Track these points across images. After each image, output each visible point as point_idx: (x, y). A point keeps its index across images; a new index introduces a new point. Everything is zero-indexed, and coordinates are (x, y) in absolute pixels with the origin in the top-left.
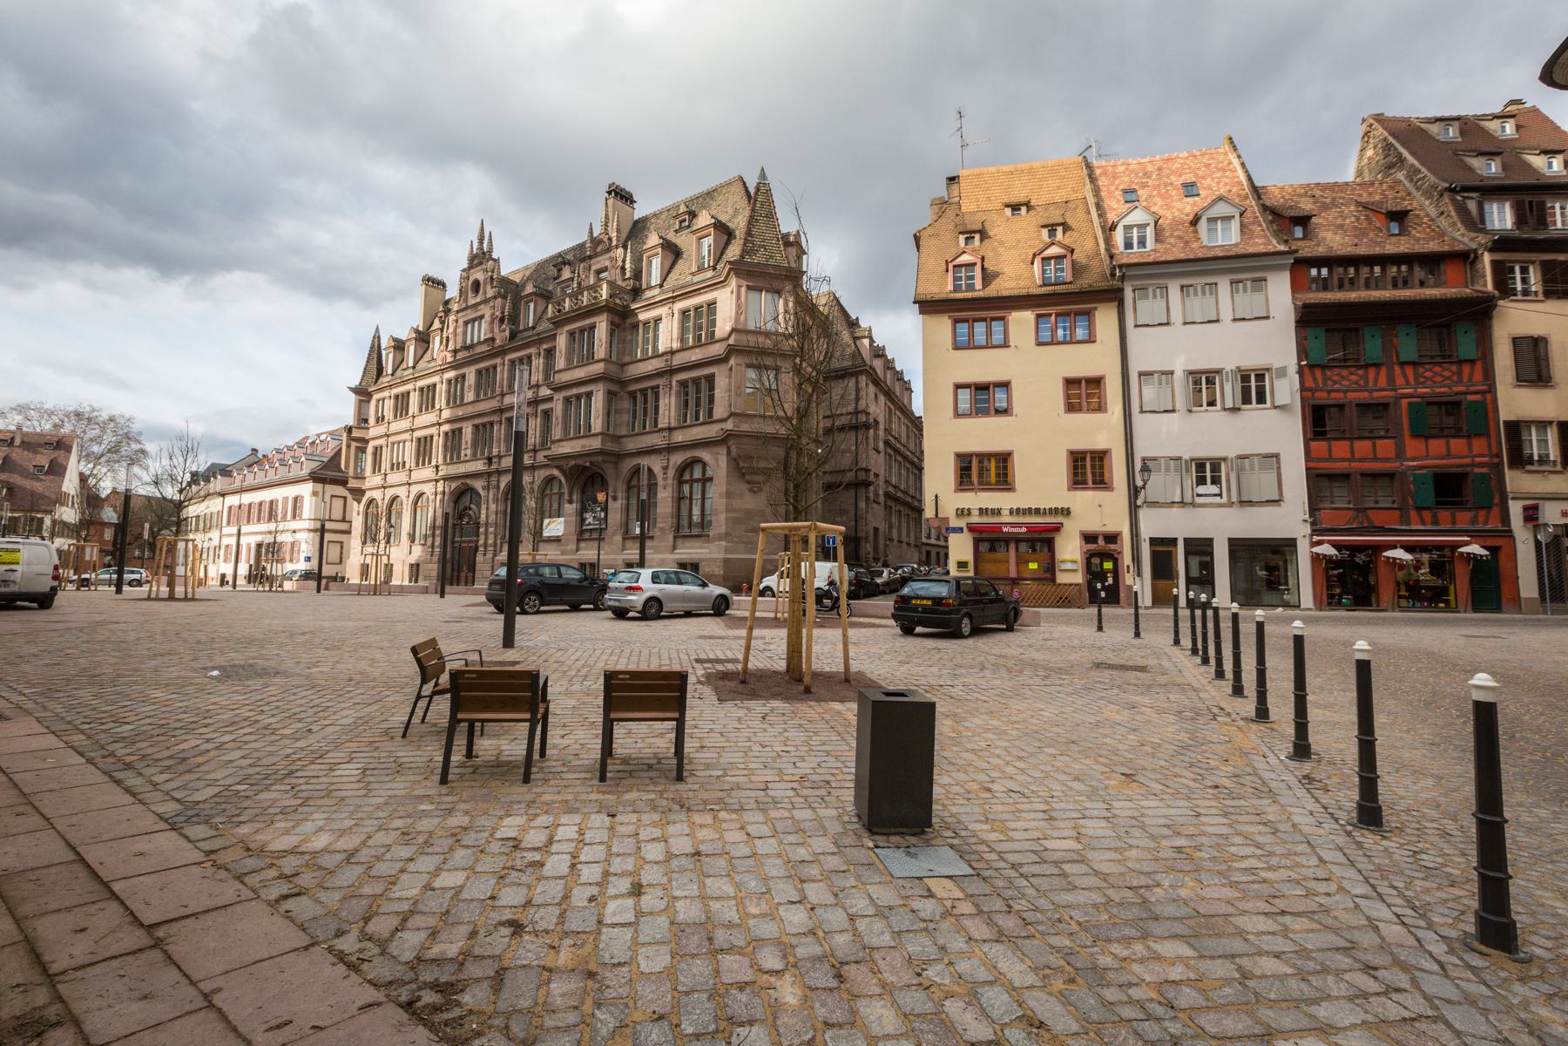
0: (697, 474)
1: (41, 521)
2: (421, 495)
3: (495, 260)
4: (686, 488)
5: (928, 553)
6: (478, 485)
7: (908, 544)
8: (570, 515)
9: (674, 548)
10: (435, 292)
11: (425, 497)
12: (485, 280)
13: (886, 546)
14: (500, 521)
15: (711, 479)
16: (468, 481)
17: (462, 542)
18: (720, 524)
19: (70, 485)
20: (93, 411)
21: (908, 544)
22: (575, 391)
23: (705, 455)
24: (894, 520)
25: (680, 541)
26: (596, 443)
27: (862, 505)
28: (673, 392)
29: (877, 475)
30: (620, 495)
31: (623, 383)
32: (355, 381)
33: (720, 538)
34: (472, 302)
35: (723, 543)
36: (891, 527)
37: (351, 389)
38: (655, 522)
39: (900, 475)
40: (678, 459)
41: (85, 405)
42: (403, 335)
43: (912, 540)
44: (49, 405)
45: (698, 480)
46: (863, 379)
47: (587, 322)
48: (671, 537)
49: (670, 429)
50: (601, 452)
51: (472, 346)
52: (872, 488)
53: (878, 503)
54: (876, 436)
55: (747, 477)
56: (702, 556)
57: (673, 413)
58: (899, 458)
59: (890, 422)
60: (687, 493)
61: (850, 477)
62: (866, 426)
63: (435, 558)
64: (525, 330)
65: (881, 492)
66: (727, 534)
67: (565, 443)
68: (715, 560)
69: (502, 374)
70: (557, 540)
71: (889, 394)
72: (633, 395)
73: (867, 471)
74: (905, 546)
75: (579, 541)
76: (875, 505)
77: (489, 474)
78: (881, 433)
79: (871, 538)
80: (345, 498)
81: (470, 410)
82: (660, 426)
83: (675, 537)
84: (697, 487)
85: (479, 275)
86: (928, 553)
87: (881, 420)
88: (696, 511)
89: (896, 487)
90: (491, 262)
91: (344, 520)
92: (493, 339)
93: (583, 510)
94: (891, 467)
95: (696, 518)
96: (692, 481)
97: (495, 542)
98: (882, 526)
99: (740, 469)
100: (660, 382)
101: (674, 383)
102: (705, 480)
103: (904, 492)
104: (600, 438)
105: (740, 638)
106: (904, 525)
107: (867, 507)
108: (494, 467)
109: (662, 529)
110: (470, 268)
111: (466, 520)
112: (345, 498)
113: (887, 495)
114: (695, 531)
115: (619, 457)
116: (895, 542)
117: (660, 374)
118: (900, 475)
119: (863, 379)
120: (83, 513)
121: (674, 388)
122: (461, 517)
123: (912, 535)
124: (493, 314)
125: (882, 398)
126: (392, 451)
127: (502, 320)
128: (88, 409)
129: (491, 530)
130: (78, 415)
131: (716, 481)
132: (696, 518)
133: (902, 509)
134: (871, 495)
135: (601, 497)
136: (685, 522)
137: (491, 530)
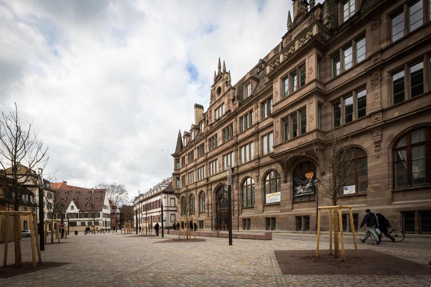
1: (99, 213)
2: (201, 192)
3: (227, 73)
8: (285, 189)
10: (199, 110)
11: (203, 193)
12: (223, 86)
14: (240, 199)
16: (222, 182)
17: (221, 210)
19: (106, 203)
20: (115, 184)
22: (290, 111)
25: (265, 208)
32: (174, 152)
34: (217, 98)
41: (113, 183)
42: (188, 131)
44: (106, 184)
51: (219, 119)
63: (210, 218)
64: (246, 99)
67: (284, 146)
69: (236, 126)
70: (277, 204)
75: (293, 203)
80: (175, 199)
81: (220, 149)
90: (226, 75)
91: (175, 207)
92: (230, 111)
93: (295, 185)
105: (327, 238)
108: (235, 172)
111: (222, 200)
112: (175, 199)
120: (111, 211)
122: (220, 199)
126: (189, 177)
127: (234, 100)
128: (114, 184)
130: (112, 186)
135: (309, 176)
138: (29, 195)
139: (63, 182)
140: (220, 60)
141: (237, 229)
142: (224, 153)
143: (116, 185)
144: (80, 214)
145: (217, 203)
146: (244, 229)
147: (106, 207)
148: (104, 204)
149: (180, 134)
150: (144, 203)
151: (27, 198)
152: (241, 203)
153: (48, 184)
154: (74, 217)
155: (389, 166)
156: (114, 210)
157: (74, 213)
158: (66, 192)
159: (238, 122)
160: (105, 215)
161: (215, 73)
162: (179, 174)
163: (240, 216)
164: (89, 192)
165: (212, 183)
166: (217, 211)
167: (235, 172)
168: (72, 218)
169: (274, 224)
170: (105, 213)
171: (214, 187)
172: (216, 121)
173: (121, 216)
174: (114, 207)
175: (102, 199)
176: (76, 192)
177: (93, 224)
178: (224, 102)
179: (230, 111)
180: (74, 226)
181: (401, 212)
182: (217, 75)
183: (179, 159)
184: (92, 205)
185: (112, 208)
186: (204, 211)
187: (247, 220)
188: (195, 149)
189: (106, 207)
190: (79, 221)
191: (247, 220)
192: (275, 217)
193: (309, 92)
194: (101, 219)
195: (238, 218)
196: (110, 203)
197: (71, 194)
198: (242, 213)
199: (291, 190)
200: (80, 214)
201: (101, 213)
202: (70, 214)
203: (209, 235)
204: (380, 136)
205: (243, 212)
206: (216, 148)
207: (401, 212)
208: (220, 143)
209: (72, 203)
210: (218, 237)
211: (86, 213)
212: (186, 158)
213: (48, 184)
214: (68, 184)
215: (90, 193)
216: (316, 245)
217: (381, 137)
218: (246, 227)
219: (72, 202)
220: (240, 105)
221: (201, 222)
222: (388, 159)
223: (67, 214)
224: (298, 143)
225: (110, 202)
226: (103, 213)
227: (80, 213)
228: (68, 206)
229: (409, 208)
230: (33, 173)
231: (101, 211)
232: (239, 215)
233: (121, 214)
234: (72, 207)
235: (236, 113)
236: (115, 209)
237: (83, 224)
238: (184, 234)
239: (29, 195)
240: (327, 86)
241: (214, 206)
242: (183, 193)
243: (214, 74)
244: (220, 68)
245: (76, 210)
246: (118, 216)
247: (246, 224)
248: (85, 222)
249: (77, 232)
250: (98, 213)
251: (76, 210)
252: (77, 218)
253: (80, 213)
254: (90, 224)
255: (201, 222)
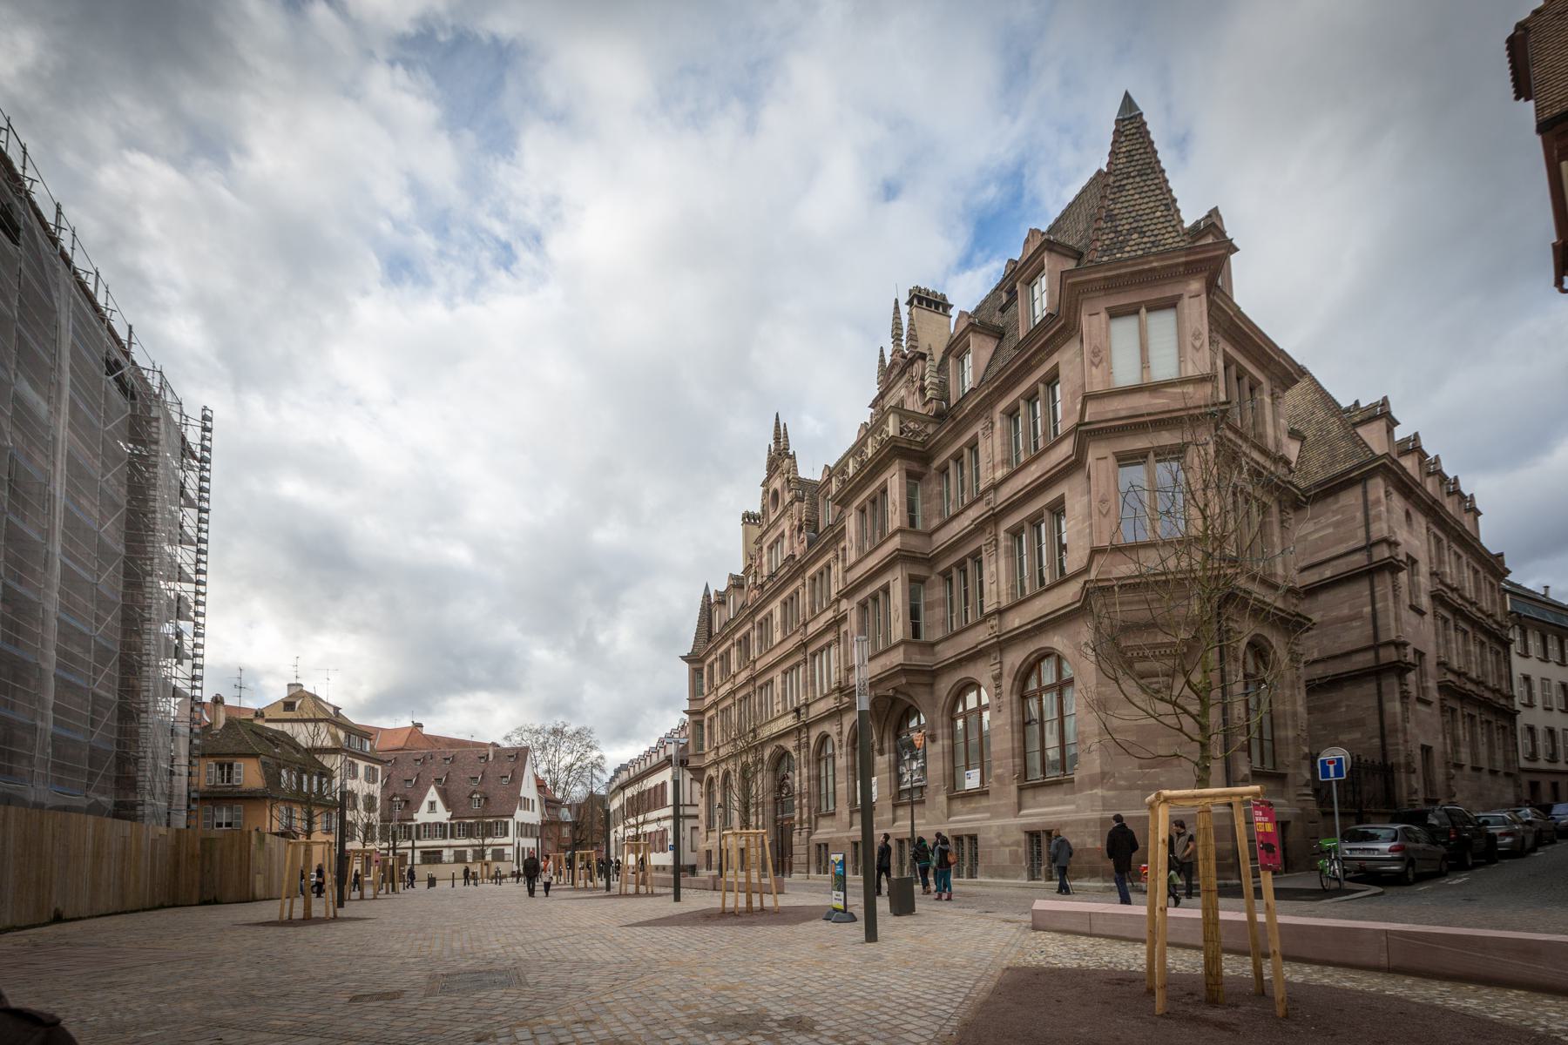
0: (1049, 677)
1: (507, 823)
4: (1033, 705)
5: (1534, 786)
6: (790, 744)
7: (1493, 772)
9: (1020, 807)
12: (783, 487)
13: (1450, 778)
14: (814, 790)
15: (1071, 682)
17: (783, 820)
18: (1090, 763)
19: (528, 790)
20: (565, 726)
21: (1493, 772)
22: (869, 590)
23: (1056, 641)
24: (1462, 731)
25: (1028, 795)
26: (897, 657)
27: (1394, 707)
28: (1002, 550)
29: (1420, 654)
30: (939, 732)
31: (930, 561)
32: (687, 650)
33: (1094, 782)
35: (1098, 791)
36: (1456, 744)
37: (682, 658)
38: (990, 769)
39: (1467, 653)
40: (1015, 658)
43: (1499, 765)
45: (1050, 688)
46: (1377, 487)
47: (877, 483)
48: (1013, 788)
49: (1000, 612)
50: (904, 670)
52: (1411, 677)
53: (1428, 703)
54: (1414, 588)
55: (1138, 666)
56: (1065, 818)
57: (1003, 586)
58: (1462, 625)
59: (1441, 562)
60: (1035, 713)
61: (1364, 660)
62: (1392, 567)
65: (1431, 684)
66: (1103, 775)
68: (1087, 823)
71: (1432, 511)
72: (946, 576)
73: (1400, 645)
74: (1486, 777)
75: (895, 806)
76: (1420, 707)
77: (799, 730)
78: (1424, 580)
79: (1418, 763)
81: (778, 653)
82: (986, 610)
83: (1020, 789)
84: (1049, 700)
85: (777, 484)
86: (1534, 786)
87: (1422, 558)
88: (1052, 741)
89: (1458, 674)
92: (793, 556)
94: (1447, 642)
95: (1053, 754)
96: (1043, 690)
97: (809, 817)
98: (1438, 744)
99: (1122, 652)
100: (981, 541)
101: (1002, 535)
102: (1062, 685)
103: (1477, 683)
104: (901, 649)
106: (1482, 739)
107: (1405, 709)
109: (999, 778)
110: (769, 477)
113: (1443, 687)
114: (1053, 775)
115: (931, 675)
116: (1467, 769)
117: (979, 527)
118: (1467, 653)
119: (1377, 487)
120: (543, 815)
121: (1002, 544)
122: (780, 788)
123: (1499, 756)
124: (792, 525)
125: (1420, 521)
127: (800, 529)
129: (805, 801)
131: (1078, 684)
132: (1053, 754)
133: (1475, 712)
134: (1412, 689)
136: (1035, 762)
137: (805, 801)
138: (321, 775)
139: (410, 724)
140: (777, 419)
141: (805, 870)
142: (786, 666)
143: (566, 729)
144: (452, 825)
145: (776, 799)
146: (1033, 878)
147: (526, 804)
148: (522, 795)
149: (707, 595)
150: (630, 792)
151: (315, 782)
152: (814, 804)
153: (368, 743)
154: (436, 836)
155: (1013, 732)
156: (551, 811)
157: (436, 824)
158: (416, 760)
159: (807, 588)
160: (525, 830)
161: (882, 355)
162: (702, 713)
163: (813, 837)
164: (481, 758)
165: (763, 744)
166: (776, 821)
167: (803, 718)
168: (431, 837)
169: (975, 857)
170: (523, 824)
171: (767, 753)
172: (771, 576)
173: (573, 833)
174: (551, 804)
175: (516, 779)
176: (446, 759)
177: (488, 858)
178: (783, 532)
179: (793, 556)
180: (435, 863)
181: (1026, 832)
182: (888, 362)
183: (702, 669)
184: (486, 799)
185: (547, 807)
186: (831, 808)
187: (966, 840)
188: (733, 644)
189: (526, 804)
190: (450, 847)
191: (966, 840)
192: (976, 835)
193: (1060, 463)
194: (511, 842)
195: (808, 841)
196: (539, 791)
197: (432, 764)
198: (816, 829)
199: (892, 774)
200: (452, 825)
201: (511, 821)
202: (425, 825)
203: (701, 885)
204: (998, 666)
205: (819, 825)
206: (771, 650)
207: (1026, 832)
208: (778, 637)
209: (432, 794)
210: (715, 889)
211: (468, 824)
212: (717, 666)
213: (368, 743)
214: (426, 731)
215: (483, 761)
216: (720, 901)
217: (1001, 668)
218: (1043, 868)
219: (432, 789)
220: (811, 544)
221: (823, 847)
222: (1012, 717)
223: (418, 826)
224: (882, 667)
225: (541, 786)
226: (518, 823)
227: (454, 822)
228: (421, 802)
229: (1034, 824)
230: (331, 711)
231: (512, 816)
232: (810, 834)
233: (576, 826)
234: (432, 804)
235: (802, 566)
236: (555, 808)
237: (460, 857)
238: (774, 891)
239: (321, 775)
240: (935, 537)
241: (769, 807)
242: (709, 766)
243: (767, 452)
244: (897, 337)
245: (442, 815)
246: (566, 832)
247: (1039, 853)
248: (465, 851)
249: (435, 879)
250: (501, 822)
251: (442, 815)
252: (445, 837)
253: (454, 822)
254: (480, 855)
255: (823, 847)
